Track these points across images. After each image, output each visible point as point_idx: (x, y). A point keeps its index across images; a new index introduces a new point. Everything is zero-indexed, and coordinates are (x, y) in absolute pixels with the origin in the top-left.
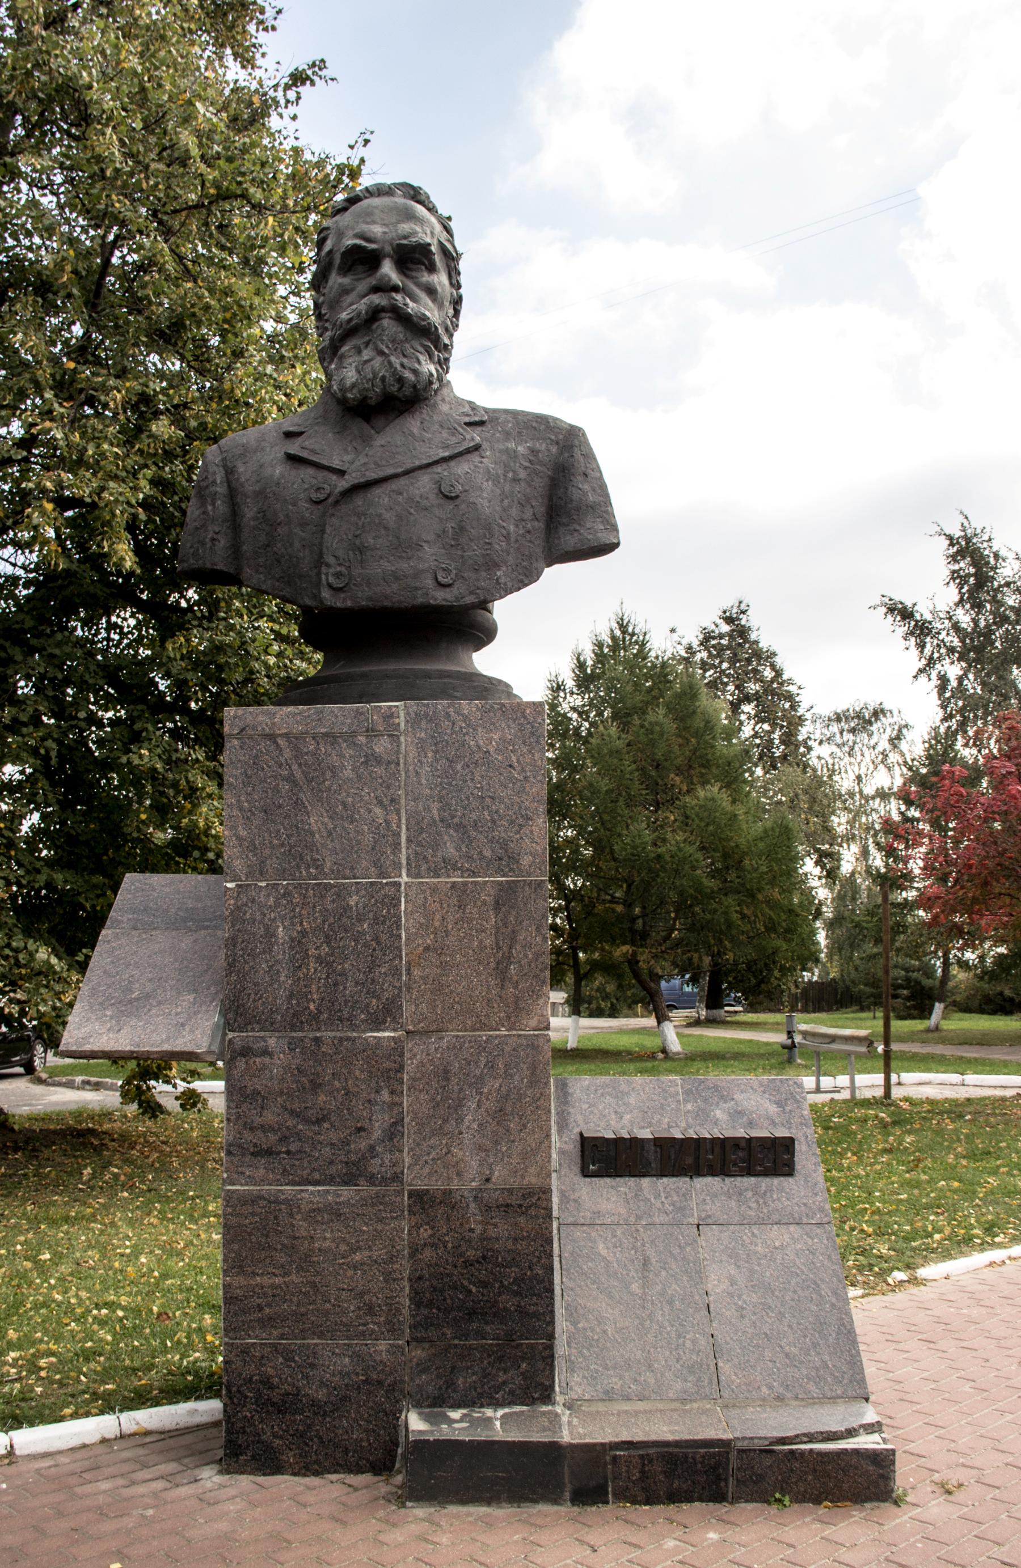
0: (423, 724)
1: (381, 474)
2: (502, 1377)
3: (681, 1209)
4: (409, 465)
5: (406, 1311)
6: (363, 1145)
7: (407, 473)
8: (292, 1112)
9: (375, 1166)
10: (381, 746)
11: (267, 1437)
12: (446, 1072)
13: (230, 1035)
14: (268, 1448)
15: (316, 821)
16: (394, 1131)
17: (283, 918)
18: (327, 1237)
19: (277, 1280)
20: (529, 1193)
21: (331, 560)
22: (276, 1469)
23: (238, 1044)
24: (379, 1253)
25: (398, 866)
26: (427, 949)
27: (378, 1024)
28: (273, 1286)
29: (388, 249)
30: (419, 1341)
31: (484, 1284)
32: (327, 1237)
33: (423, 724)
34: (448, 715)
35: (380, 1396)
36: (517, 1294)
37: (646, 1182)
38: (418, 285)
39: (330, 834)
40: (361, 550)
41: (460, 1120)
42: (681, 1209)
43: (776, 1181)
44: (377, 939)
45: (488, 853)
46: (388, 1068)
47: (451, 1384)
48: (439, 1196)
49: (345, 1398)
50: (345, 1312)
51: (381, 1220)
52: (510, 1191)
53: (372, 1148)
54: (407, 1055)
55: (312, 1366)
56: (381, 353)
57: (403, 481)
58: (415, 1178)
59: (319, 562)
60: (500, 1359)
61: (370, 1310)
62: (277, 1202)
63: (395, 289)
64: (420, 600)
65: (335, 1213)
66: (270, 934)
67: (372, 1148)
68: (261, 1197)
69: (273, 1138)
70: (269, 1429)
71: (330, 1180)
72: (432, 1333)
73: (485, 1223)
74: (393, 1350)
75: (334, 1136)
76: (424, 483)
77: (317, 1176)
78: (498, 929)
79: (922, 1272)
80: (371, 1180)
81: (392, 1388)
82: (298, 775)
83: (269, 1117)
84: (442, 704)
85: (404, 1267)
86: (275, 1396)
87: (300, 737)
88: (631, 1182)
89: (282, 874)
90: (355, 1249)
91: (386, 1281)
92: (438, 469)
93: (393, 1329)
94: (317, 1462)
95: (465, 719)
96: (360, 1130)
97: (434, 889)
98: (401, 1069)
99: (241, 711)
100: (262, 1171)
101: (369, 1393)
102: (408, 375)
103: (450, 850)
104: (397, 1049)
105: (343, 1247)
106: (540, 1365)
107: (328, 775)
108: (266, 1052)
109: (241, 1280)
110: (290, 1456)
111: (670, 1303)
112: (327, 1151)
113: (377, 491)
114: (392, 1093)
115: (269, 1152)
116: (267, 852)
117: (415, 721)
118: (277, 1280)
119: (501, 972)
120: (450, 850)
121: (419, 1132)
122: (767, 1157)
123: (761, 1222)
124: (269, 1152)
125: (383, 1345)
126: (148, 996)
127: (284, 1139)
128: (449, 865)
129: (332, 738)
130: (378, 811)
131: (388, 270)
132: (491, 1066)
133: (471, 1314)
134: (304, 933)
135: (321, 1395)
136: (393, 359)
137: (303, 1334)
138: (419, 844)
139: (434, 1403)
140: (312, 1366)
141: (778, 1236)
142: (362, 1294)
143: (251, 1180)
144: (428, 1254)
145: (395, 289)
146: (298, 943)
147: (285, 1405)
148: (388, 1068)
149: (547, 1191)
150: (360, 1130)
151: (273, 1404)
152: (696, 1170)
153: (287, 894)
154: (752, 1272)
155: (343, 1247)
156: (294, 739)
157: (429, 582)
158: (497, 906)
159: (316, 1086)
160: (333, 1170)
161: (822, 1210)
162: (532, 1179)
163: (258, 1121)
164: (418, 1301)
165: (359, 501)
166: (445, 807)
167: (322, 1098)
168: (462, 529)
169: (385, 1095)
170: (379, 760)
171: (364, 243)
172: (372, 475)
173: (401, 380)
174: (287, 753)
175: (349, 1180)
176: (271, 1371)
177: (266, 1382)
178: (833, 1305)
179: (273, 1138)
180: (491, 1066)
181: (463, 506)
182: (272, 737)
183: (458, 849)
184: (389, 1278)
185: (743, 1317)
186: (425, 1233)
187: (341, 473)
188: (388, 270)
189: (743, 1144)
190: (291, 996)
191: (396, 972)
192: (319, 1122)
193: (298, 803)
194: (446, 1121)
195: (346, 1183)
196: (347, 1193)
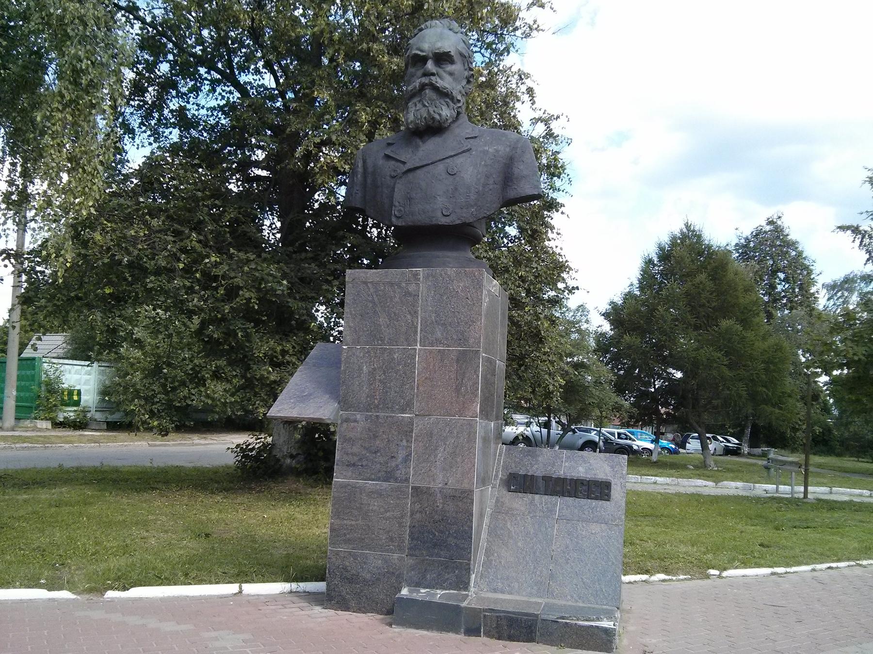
0: (430, 278)
1: (421, 164)
2: (447, 576)
3: (551, 511)
4: (435, 159)
5: (407, 542)
6: (393, 464)
7: (432, 163)
8: (365, 448)
9: (398, 474)
10: (412, 288)
11: (344, 593)
12: (431, 434)
13: (341, 412)
14: (344, 599)
15: (383, 320)
16: (407, 459)
17: (366, 363)
18: (375, 505)
19: (353, 523)
20: (463, 492)
21: (397, 204)
22: (347, 609)
23: (345, 417)
24: (397, 514)
25: (415, 341)
26: (426, 378)
27: (403, 411)
28: (351, 525)
29: (431, 55)
30: (411, 555)
31: (441, 532)
32: (375, 505)
33: (430, 278)
34: (441, 275)
35: (393, 580)
36: (456, 538)
37: (537, 497)
38: (445, 71)
39: (388, 326)
40: (410, 199)
41: (436, 456)
42: (551, 511)
43: (601, 502)
44: (405, 373)
45: (455, 337)
46: (406, 430)
47: (424, 577)
48: (425, 490)
49: (378, 579)
50: (381, 539)
51: (399, 498)
52: (456, 490)
53: (397, 466)
54: (415, 425)
55: (365, 563)
56: (424, 106)
57: (430, 167)
58: (413, 481)
59: (392, 205)
60: (446, 568)
61: (391, 539)
62: (356, 487)
63: (433, 74)
64: (434, 223)
65: (379, 494)
66: (360, 369)
67: (397, 466)
68: (349, 485)
69: (356, 458)
70: (345, 590)
71: (378, 479)
72: (417, 552)
73: (444, 504)
74: (401, 559)
75: (381, 460)
76: (441, 167)
77: (373, 477)
78: (457, 371)
79: (725, 574)
80: (396, 480)
81: (398, 576)
82: (376, 299)
83: (355, 449)
84: (438, 270)
85: (407, 521)
86: (348, 575)
87: (377, 283)
88: (530, 496)
89: (367, 343)
90: (386, 511)
91: (399, 526)
92: (448, 161)
93: (400, 549)
94: (364, 607)
95: (449, 277)
96: (393, 457)
97: (431, 352)
98: (412, 431)
99: (353, 271)
100: (350, 473)
101: (388, 578)
102: (437, 117)
103: (439, 335)
104: (411, 422)
105: (382, 510)
106: (464, 572)
107: (389, 300)
108: (355, 421)
109: (338, 522)
110: (353, 604)
111: (534, 553)
112: (378, 466)
113: (418, 172)
114: (407, 441)
115: (354, 465)
116: (361, 333)
117: (427, 277)
118: (353, 523)
119: (458, 390)
120: (439, 335)
121: (418, 460)
122: (599, 490)
123: (587, 521)
124: (354, 465)
125: (396, 556)
126: (311, 395)
127: (360, 459)
128: (438, 342)
129: (391, 284)
130: (409, 316)
131: (430, 65)
132: (451, 432)
133: (435, 545)
134: (374, 369)
135: (368, 576)
136: (430, 108)
137: (362, 548)
138: (426, 332)
139: (417, 585)
140: (365, 563)
141: (595, 528)
142: (389, 532)
143: (345, 477)
144: (418, 516)
145: (433, 74)
146: (372, 373)
147: (352, 580)
148: (406, 430)
149: (472, 491)
150: (393, 457)
151: (348, 579)
152: (562, 493)
153: (368, 352)
154: (577, 543)
155: (382, 510)
156: (375, 284)
157: (439, 214)
158: (458, 361)
159: (375, 437)
160: (380, 475)
161: (620, 518)
162: (466, 486)
163: (350, 451)
164: (411, 534)
165: (410, 176)
166: (438, 315)
167: (378, 442)
168: (456, 189)
169: (404, 443)
170: (410, 294)
171: (419, 53)
172: (418, 165)
173: (433, 118)
174: (372, 290)
175: (386, 480)
176: (348, 564)
177: (345, 569)
178: (613, 563)
179: (356, 458)
180: (451, 432)
181: (457, 179)
182: (365, 283)
183: (442, 334)
184: (401, 525)
185: (567, 563)
186: (417, 506)
187: (404, 163)
188: (430, 65)
189: (585, 483)
190: (368, 396)
191: (412, 388)
192: (375, 453)
193: (375, 312)
194: (430, 456)
195: (385, 481)
196: (385, 485)
